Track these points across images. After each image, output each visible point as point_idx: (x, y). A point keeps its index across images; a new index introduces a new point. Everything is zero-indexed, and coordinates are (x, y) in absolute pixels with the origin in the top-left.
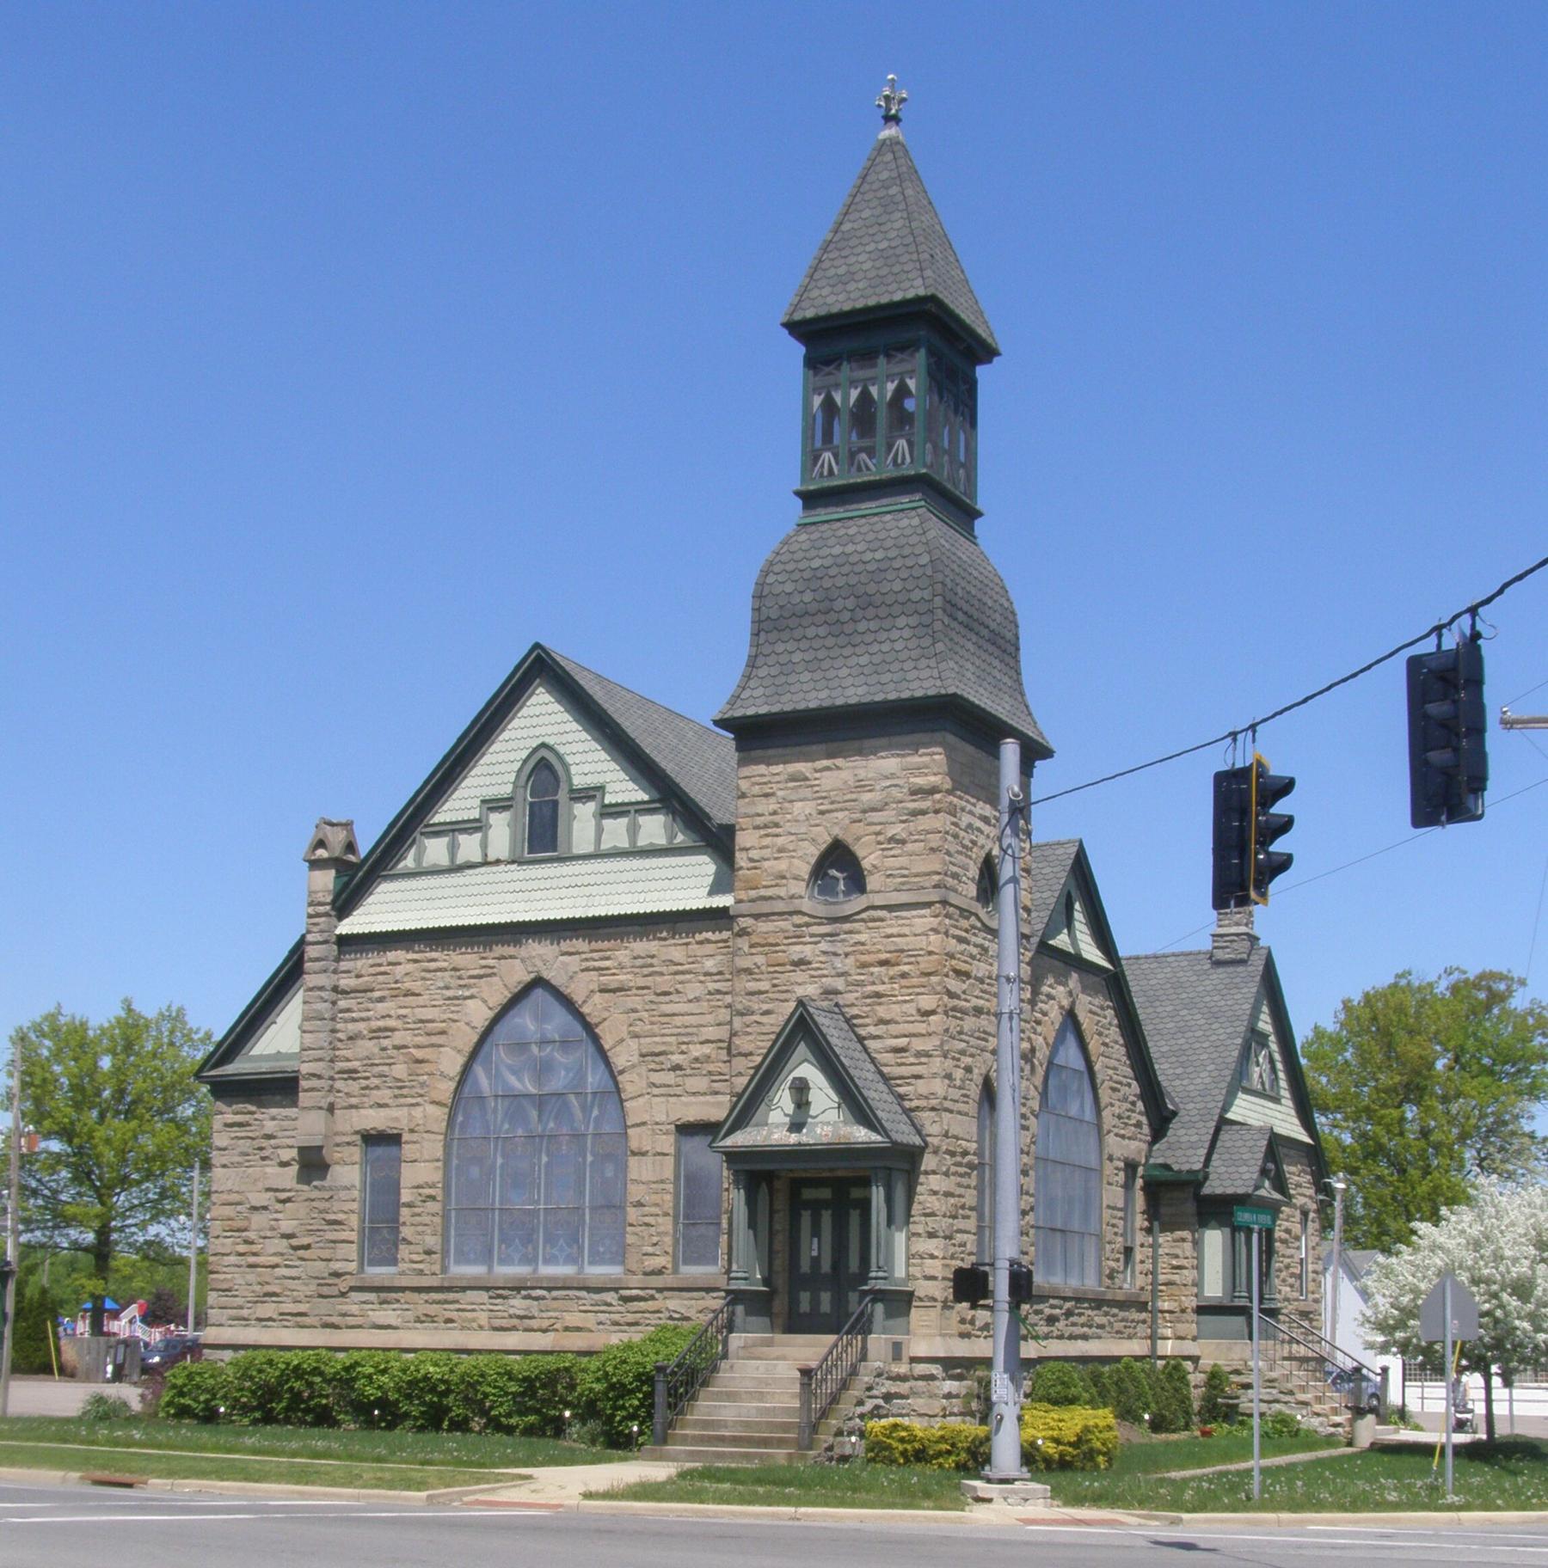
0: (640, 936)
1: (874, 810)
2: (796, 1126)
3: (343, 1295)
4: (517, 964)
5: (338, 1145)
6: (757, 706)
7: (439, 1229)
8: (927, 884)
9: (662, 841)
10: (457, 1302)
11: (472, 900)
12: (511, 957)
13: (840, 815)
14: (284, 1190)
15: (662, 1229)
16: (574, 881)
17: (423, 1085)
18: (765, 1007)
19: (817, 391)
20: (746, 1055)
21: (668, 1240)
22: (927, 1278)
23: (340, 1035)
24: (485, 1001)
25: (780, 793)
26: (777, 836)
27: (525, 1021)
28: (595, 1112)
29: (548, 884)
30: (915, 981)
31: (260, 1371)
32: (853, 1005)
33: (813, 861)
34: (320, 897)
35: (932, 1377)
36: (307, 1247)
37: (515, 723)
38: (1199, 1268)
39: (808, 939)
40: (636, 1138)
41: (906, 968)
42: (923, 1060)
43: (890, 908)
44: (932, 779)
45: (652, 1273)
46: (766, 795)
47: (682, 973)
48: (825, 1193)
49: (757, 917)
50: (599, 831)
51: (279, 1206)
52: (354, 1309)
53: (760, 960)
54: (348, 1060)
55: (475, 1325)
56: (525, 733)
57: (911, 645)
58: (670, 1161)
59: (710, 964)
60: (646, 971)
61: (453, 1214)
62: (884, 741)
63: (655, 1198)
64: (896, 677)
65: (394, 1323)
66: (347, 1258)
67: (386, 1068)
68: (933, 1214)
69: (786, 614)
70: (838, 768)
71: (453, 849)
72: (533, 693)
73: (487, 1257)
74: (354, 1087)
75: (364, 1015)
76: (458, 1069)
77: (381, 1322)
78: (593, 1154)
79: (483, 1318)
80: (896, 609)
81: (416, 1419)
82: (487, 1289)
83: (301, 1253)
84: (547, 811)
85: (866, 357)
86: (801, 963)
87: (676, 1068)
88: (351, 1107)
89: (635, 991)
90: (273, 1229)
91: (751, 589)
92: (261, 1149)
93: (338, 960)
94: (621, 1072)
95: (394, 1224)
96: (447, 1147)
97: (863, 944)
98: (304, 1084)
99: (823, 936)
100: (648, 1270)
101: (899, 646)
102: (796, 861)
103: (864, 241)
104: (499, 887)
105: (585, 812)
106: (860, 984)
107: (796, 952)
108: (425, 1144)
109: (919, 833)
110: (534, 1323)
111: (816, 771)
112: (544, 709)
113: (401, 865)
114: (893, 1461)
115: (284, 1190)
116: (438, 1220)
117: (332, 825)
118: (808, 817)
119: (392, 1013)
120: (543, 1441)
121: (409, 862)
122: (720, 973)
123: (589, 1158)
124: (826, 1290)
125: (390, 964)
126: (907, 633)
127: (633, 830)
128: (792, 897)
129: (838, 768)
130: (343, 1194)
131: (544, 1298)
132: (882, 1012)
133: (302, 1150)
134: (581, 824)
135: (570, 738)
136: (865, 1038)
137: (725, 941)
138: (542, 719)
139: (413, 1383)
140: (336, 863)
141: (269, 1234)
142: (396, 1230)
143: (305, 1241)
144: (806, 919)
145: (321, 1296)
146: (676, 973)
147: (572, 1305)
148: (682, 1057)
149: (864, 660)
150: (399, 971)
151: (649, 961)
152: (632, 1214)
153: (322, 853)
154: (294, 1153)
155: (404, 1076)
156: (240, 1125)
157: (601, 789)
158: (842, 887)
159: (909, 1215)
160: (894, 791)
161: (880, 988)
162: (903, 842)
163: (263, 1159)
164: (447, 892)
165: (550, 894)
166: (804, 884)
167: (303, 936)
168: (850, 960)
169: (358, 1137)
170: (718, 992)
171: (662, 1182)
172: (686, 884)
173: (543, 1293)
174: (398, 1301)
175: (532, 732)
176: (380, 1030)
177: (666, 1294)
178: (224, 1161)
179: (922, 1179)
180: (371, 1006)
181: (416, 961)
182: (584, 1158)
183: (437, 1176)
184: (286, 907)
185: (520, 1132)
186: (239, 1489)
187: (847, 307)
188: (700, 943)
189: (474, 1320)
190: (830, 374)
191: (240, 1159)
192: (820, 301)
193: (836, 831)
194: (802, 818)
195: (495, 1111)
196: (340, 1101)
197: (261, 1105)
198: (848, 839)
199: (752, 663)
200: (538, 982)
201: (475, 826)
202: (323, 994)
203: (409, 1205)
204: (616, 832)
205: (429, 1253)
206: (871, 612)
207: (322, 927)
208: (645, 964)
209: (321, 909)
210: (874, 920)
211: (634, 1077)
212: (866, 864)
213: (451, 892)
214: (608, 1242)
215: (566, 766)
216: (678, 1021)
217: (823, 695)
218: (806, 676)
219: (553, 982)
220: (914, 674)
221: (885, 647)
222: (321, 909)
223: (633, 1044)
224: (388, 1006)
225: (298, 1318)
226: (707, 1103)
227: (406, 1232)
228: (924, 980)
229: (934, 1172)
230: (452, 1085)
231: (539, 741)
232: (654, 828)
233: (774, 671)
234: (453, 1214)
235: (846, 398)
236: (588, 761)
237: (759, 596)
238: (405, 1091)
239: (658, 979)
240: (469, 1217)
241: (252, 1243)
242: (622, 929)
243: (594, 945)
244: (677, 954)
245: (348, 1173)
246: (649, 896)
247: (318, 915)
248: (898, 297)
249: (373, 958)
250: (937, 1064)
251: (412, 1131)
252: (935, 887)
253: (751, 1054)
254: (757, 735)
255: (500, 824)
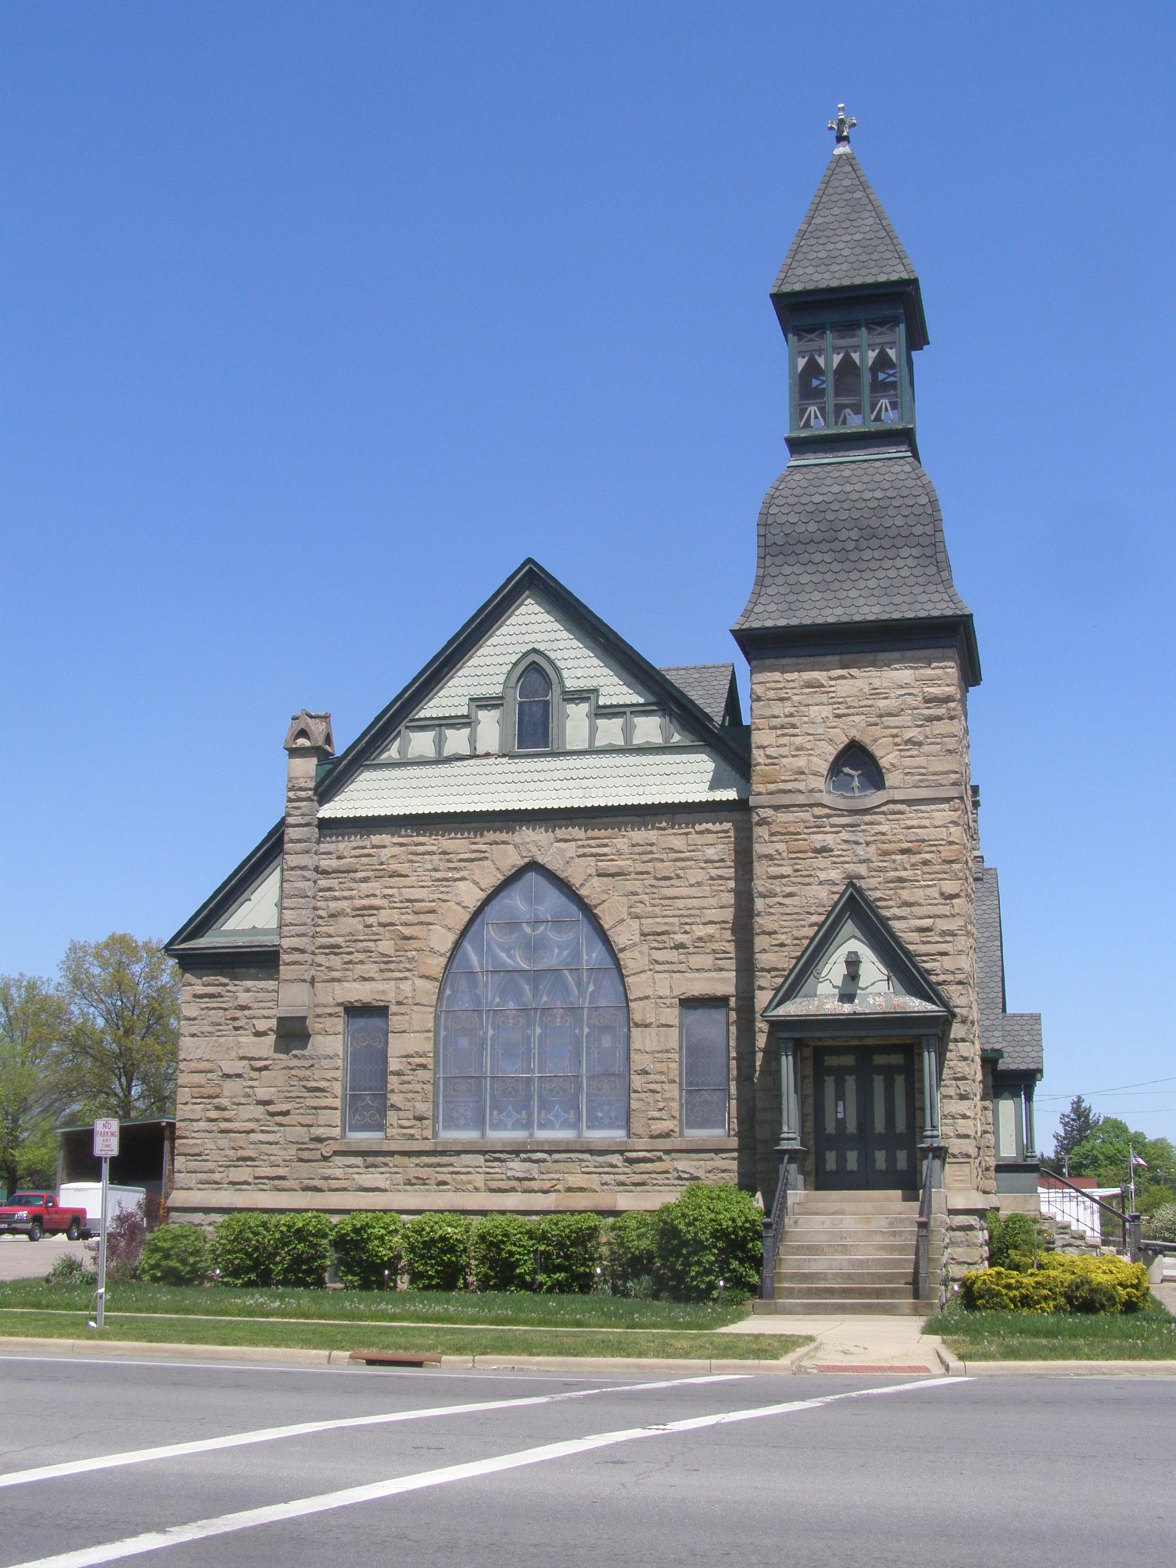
0: (642, 825)
1: (890, 715)
2: (847, 997)
3: (325, 1159)
4: (508, 852)
5: (319, 1016)
6: (771, 617)
7: (431, 1096)
8: (946, 782)
9: (658, 740)
10: (451, 1165)
11: (461, 789)
12: (504, 843)
13: (857, 718)
14: (260, 1059)
15: (667, 1095)
16: (568, 774)
17: (410, 960)
18: (788, 890)
19: (801, 354)
20: (769, 934)
21: (675, 1105)
22: (959, 1136)
23: (320, 912)
24: (476, 883)
25: (796, 698)
26: (794, 736)
27: (516, 901)
28: (591, 988)
29: (542, 776)
30: (937, 868)
31: (256, 1234)
32: (876, 889)
33: (831, 759)
34: (302, 783)
35: (971, 1228)
36: (286, 1113)
37: (504, 630)
38: (996, 1133)
39: (828, 829)
40: (639, 1011)
41: (928, 856)
42: (948, 938)
43: (909, 802)
44: (947, 689)
45: (660, 1136)
46: (782, 699)
47: (683, 860)
48: (849, 1060)
49: (776, 808)
50: (593, 730)
51: (255, 1074)
52: (339, 1172)
53: (782, 847)
54: (330, 936)
55: (470, 1187)
56: (514, 639)
57: (917, 572)
58: (675, 1032)
59: (710, 852)
60: (645, 857)
61: (441, 1081)
62: (897, 655)
63: (660, 1067)
64: (907, 599)
65: (382, 1186)
66: (331, 1123)
67: (371, 944)
68: (964, 1078)
69: (791, 541)
70: (853, 677)
71: (440, 742)
72: (522, 604)
73: (479, 1122)
74: (336, 961)
75: (346, 894)
76: (450, 945)
77: (368, 1185)
78: (589, 1026)
79: (479, 1180)
80: (899, 542)
81: (431, 1278)
82: (484, 1153)
83: (279, 1119)
84: (538, 711)
85: (848, 328)
86: (823, 850)
87: (680, 946)
88: (333, 980)
89: (633, 876)
90: (248, 1096)
91: (755, 519)
92: (234, 1019)
93: (318, 842)
94: (622, 950)
95: (382, 1095)
96: (437, 1019)
97: (884, 834)
98: (284, 957)
99: (843, 826)
100: (655, 1133)
101: (905, 572)
102: (814, 759)
103: (839, 232)
104: (491, 778)
105: (578, 712)
106: (880, 870)
107: (818, 840)
108: (415, 1016)
109: (935, 736)
110: (535, 1185)
111: (831, 679)
112: (533, 618)
113: (384, 756)
114: (1005, 1307)
115: (260, 1059)
116: (429, 1087)
117: (311, 717)
118: (825, 720)
119: (378, 892)
120: (572, 1296)
121: (393, 753)
122: (722, 860)
123: (586, 1030)
124: (852, 1150)
125: (374, 847)
126: (911, 562)
127: (628, 731)
128: (811, 791)
129: (853, 677)
130: (325, 1063)
131: (544, 1161)
132: (905, 895)
133: (281, 1020)
134: (575, 723)
135: (561, 645)
136: (889, 919)
137: (726, 832)
138: (531, 626)
139: (429, 1244)
140: (321, 754)
141: (243, 1100)
142: (384, 1097)
143: (284, 1107)
144: (828, 811)
145: (301, 1160)
146: (676, 860)
147: (576, 1167)
148: (685, 936)
149: (872, 583)
150: (385, 854)
151: (649, 848)
152: (637, 1081)
153: (302, 742)
154: (273, 1023)
155: (391, 952)
156: (212, 996)
157: (595, 691)
158: (856, 783)
159: (940, 1079)
160: (909, 699)
161: (903, 874)
162: (920, 744)
163: (236, 1029)
164: (434, 782)
165: (544, 785)
166: (823, 779)
167: (283, 819)
168: (872, 848)
169: (341, 1009)
170: (721, 877)
171: (667, 1051)
172: (691, 778)
173: (545, 1156)
174: (386, 1165)
175: (521, 639)
176: (364, 908)
177: (674, 1155)
178: (193, 1030)
179: (951, 1046)
180: (354, 885)
181: (401, 845)
182: (582, 1030)
183: (429, 1047)
184: (267, 789)
185: (511, 1005)
186: (560, 1364)
187: (834, 284)
188: (701, 833)
189: (469, 1182)
190: (811, 340)
191: (210, 1029)
192: (805, 278)
193: (853, 733)
194: (818, 720)
195: (486, 985)
196: (322, 974)
197: (234, 977)
198: (866, 740)
199: (760, 582)
200: (533, 866)
201: (465, 722)
202: (305, 873)
203: (398, 1074)
204: (611, 731)
205: (420, 1118)
206: (874, 543)
207: (304, 810)
208: (645, 851)
209: (303, 794)
210: (894, 813)
211: (637, 955)
212: (884, 763)
213: (439, 781)
214: (606, 1108)
215: (557, 670)
216: (680, 903)
217: (839, 611)
218: (816, 596)
219: (549, 866)
220: (924, 597)
221: (892, 573)
222: (303, 794)
223: (635, 924)
224: (373, 886)
225: (276, 1182)
226: (713, 979)
227: (394, 1099)
228: (946, 867)
229: (963, 1040)
230: (443, 961)
231: (530, 647)
232: (650, 728)
233: (782, 590)
234: (441, 1081)
235: (828, 362)
236: (579, 665)
237: (763, 524)
238: (392, 966)
239: (659, 865)
240: (464, 1086)
241: (225, 1109)
242: (620, 819)
243: (590, 833)
244: (678, 842)
245: (331, 1041)
246: (648, 789)
247: (299, 800)
248: (882, 278)
249: (356, 841)
250: (962, 942)
251: (400, 1003)
252: (953, 784)
253: (775, 932)
254: (761, 645)
255: (488, 721)
